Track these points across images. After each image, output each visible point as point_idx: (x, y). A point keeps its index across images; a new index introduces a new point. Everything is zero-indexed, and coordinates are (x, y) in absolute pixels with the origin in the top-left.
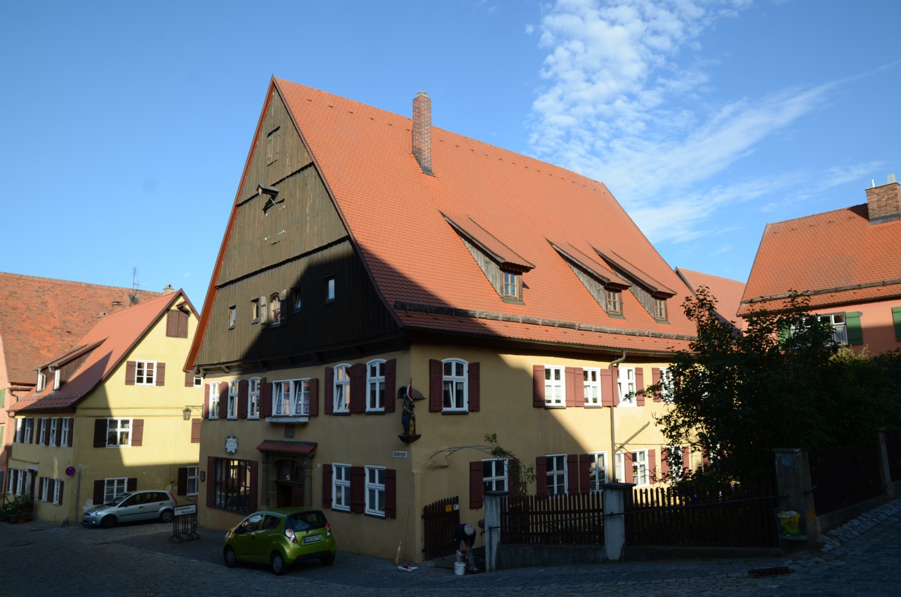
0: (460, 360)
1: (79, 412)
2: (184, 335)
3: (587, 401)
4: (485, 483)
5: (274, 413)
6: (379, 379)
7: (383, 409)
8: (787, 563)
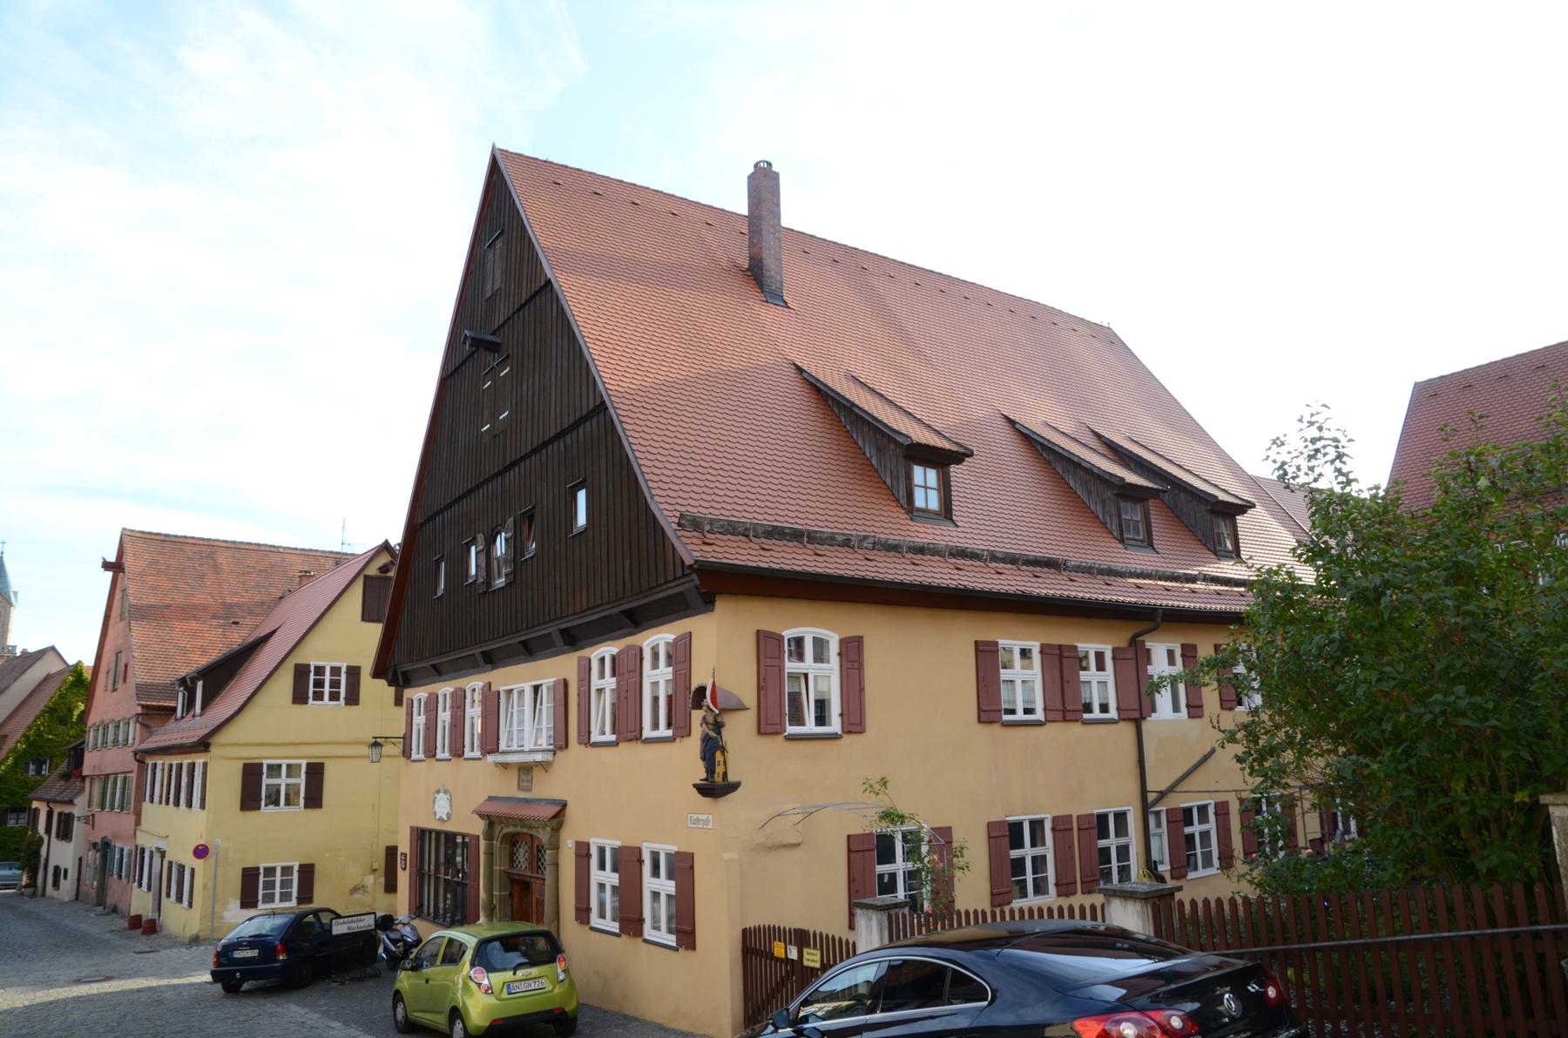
0: (822, 632)
1: (214, 750)
3: (1088, 708)
4: (881, 876)
5: (503, 747)
6: (664, 673)
7: (670, 733)
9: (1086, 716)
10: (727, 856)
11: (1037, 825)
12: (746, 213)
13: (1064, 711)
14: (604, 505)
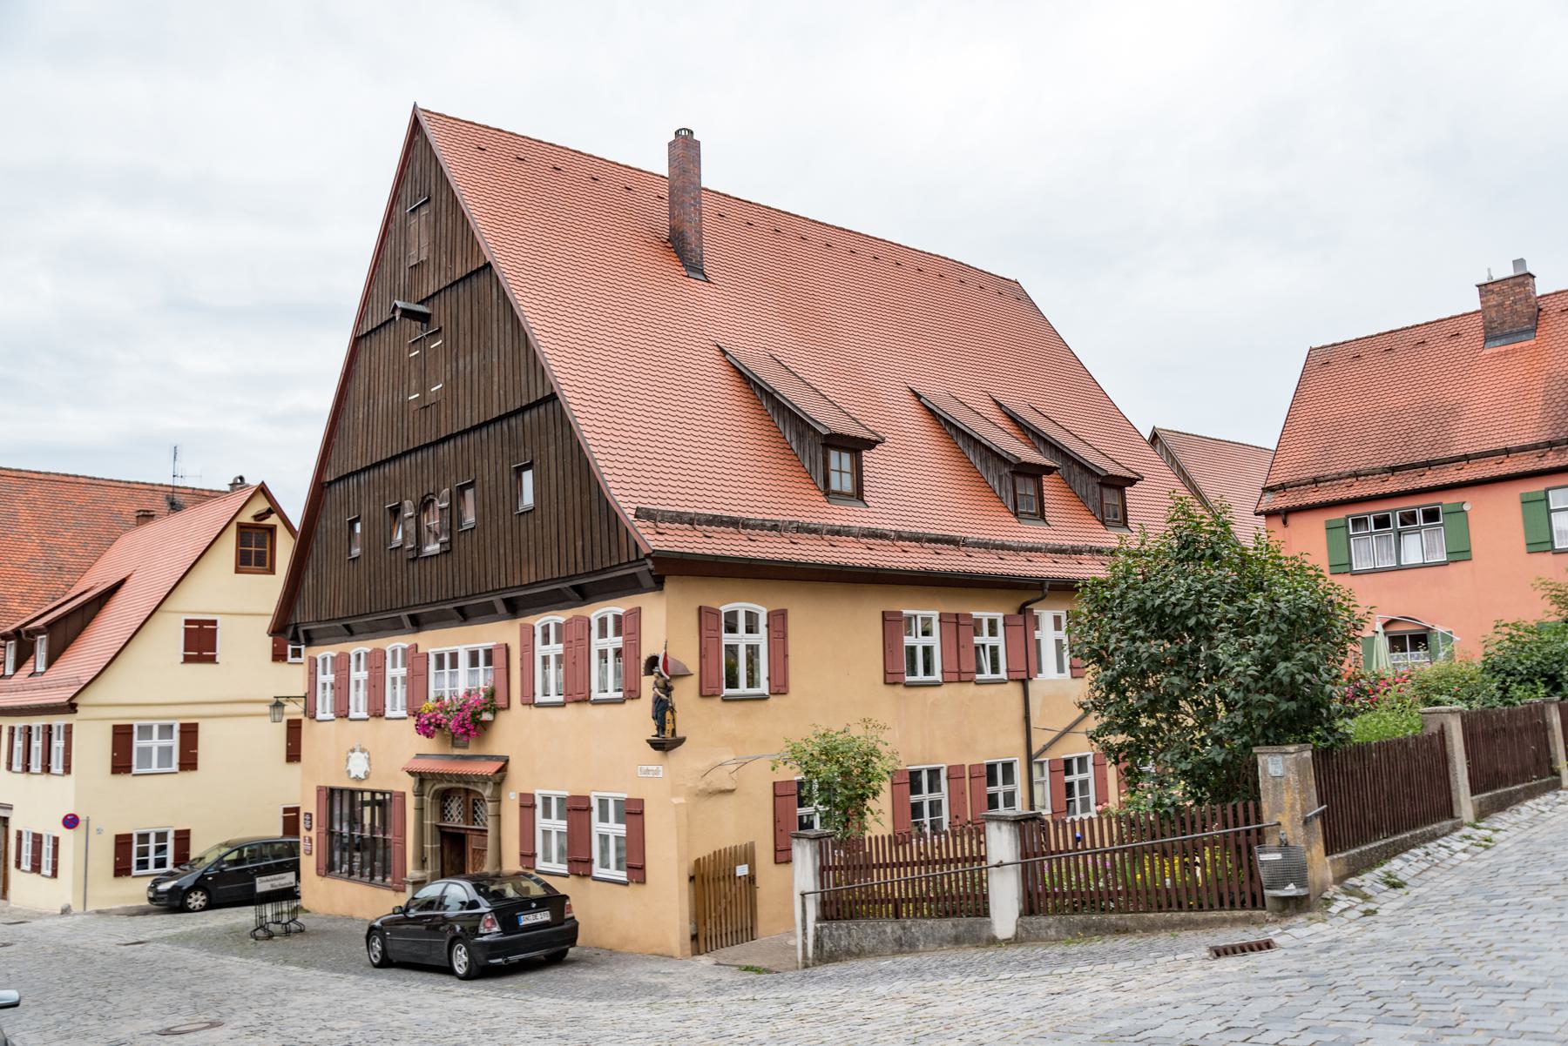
2: (272, 571)
4: (801, 818)
7: (620, 695)
8: (1273, 932)
9: (978, 677)
10: (675, 801)
11: (934, 774)
12: (664, 170)
13: (959, 672)
14: (553, 488)
